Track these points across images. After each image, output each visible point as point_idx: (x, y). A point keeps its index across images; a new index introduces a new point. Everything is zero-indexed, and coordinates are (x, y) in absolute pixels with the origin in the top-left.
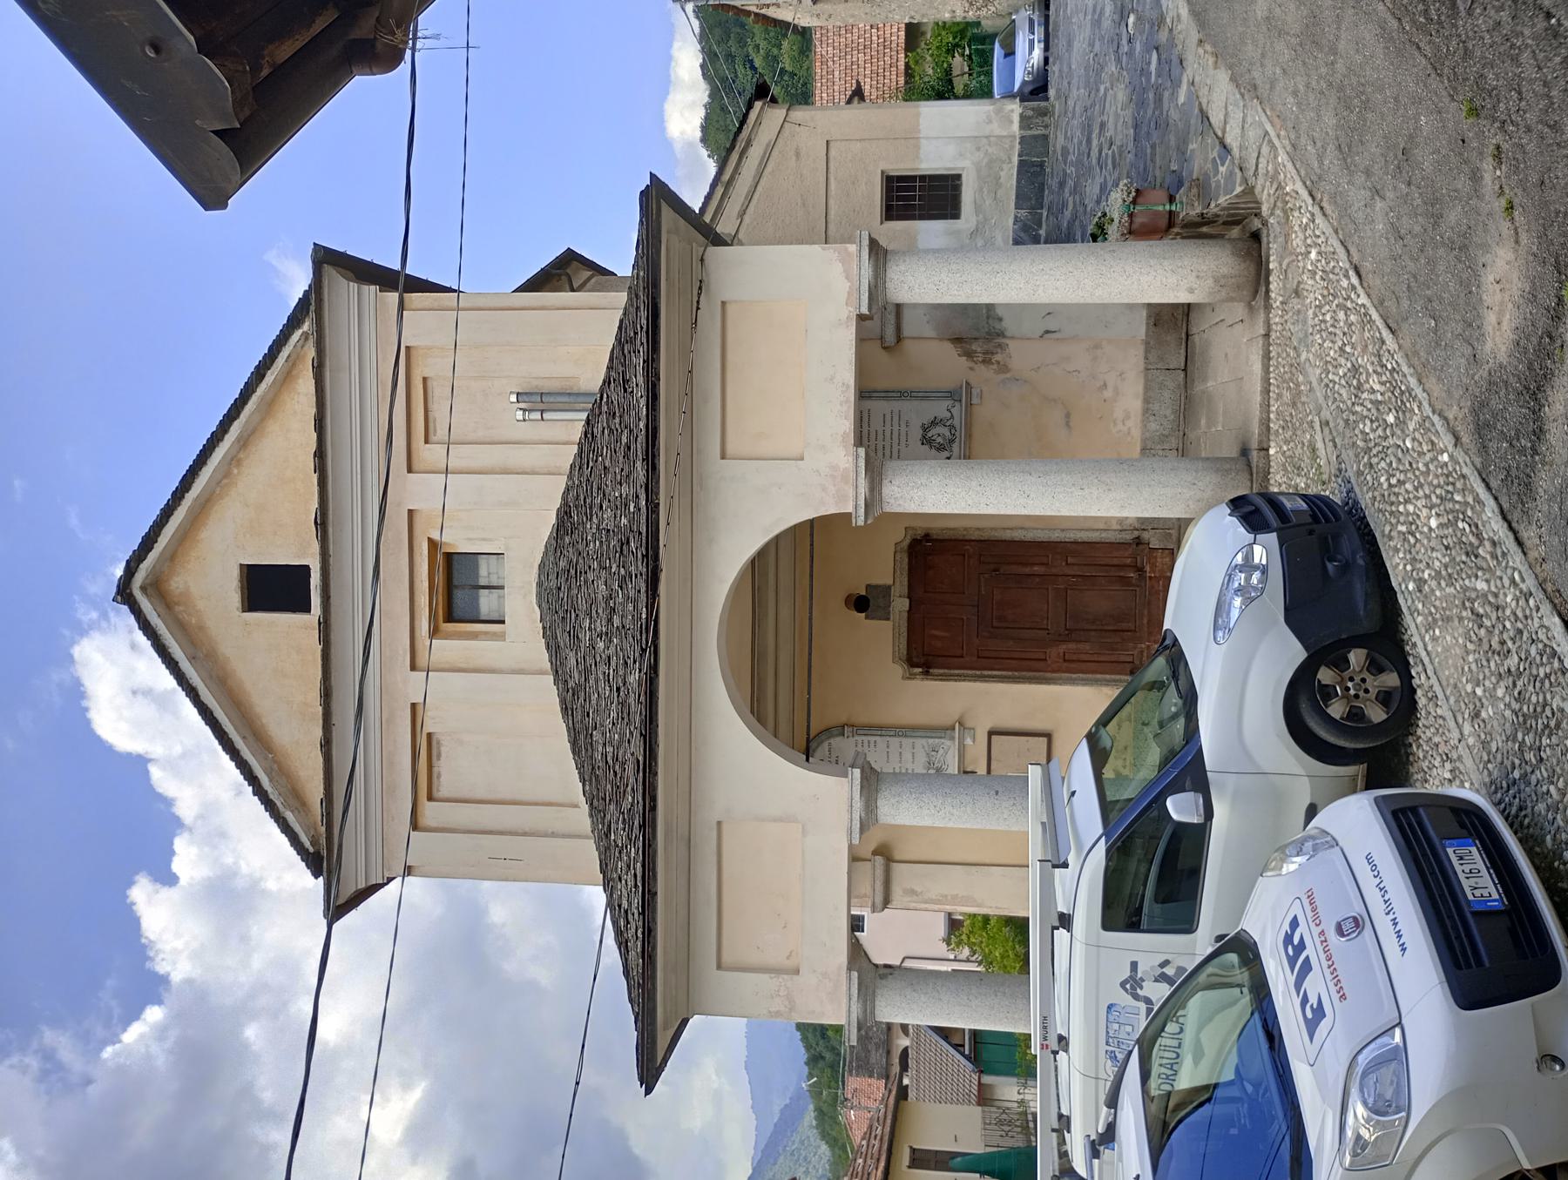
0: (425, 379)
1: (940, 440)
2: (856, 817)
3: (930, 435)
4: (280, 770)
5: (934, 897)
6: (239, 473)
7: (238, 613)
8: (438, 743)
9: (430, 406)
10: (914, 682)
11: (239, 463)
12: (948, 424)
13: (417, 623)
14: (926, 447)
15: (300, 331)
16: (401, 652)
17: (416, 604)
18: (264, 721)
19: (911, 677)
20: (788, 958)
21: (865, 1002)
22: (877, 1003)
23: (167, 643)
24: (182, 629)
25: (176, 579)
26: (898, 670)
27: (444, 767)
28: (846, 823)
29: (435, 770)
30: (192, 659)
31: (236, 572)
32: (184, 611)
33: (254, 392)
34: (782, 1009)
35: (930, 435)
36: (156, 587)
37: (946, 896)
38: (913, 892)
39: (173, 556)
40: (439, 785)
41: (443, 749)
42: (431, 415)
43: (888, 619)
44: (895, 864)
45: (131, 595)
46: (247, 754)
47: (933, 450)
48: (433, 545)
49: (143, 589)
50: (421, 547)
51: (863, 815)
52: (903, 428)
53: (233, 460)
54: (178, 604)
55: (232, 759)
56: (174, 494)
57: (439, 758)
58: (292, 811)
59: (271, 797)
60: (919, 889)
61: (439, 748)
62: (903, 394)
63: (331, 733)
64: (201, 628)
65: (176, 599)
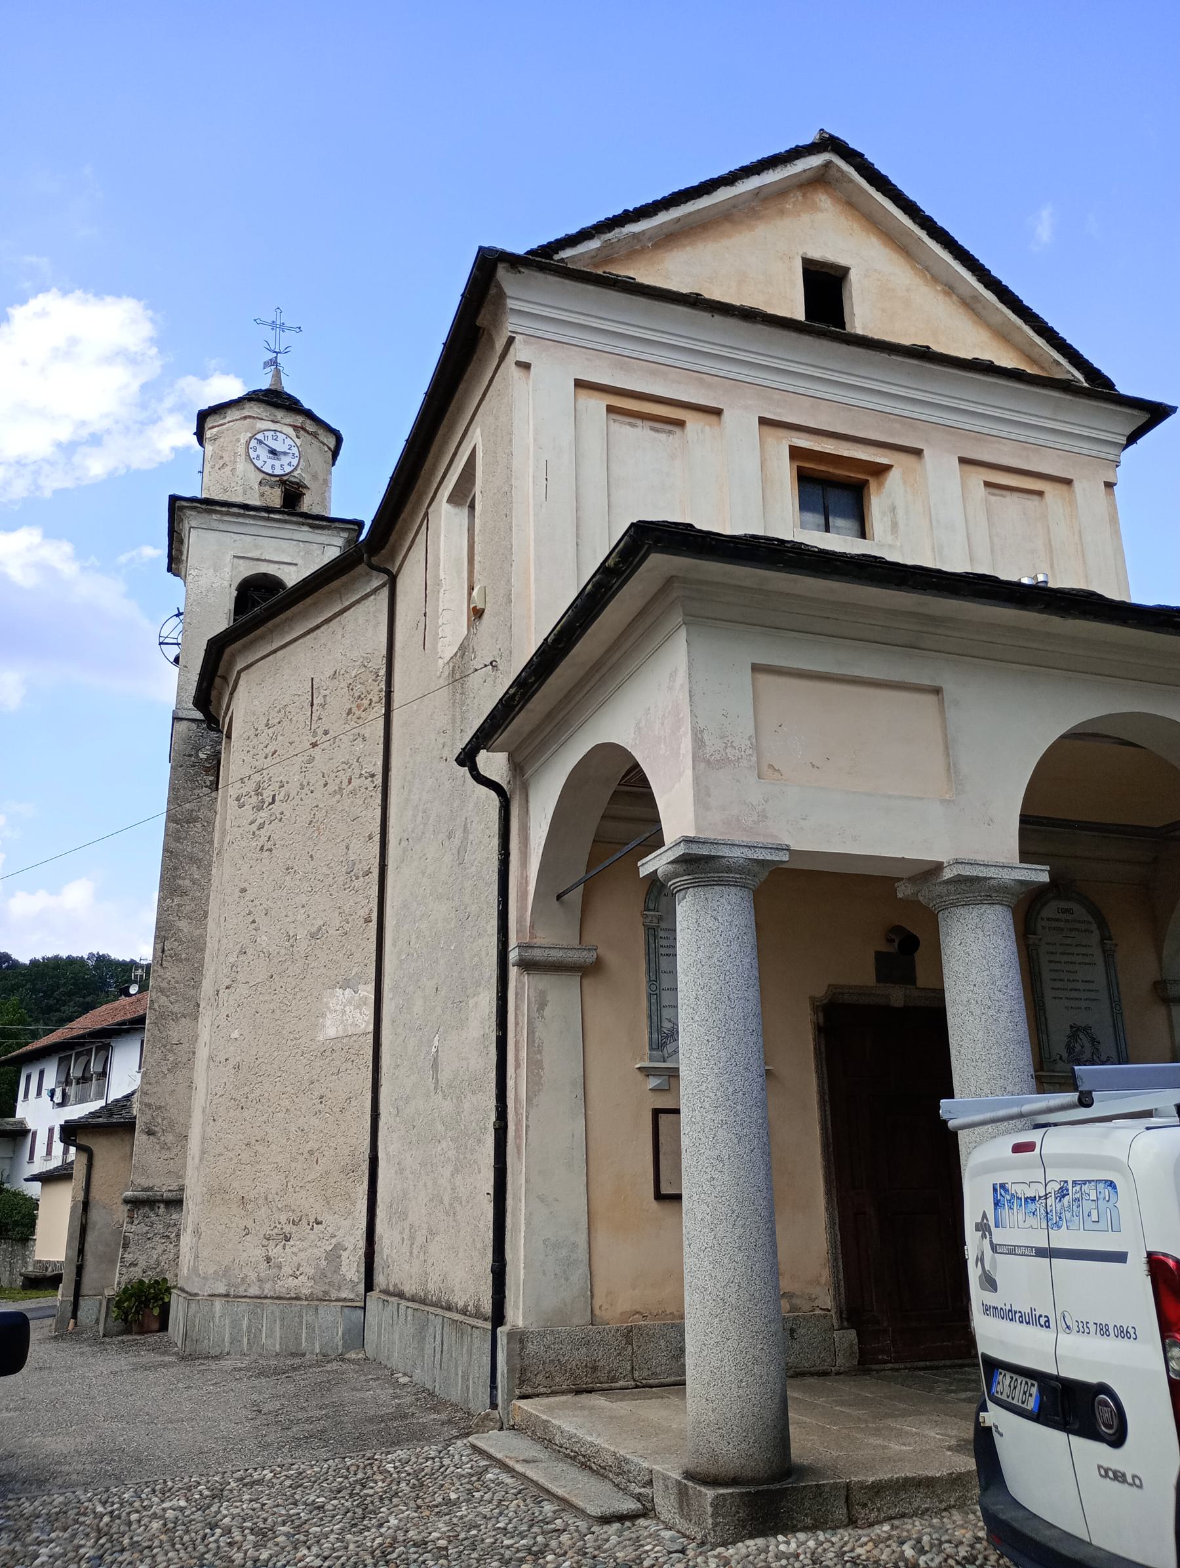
0: (1040, 494)
1: (1078, 1048)
2: (991, 873)
3: (1081, 1036)
4: (670, 238)
5: (537, 1034)
6: (937, 290)
7: (801, 253)
8: (670, 432)
9: (1016, 495)
10: (809, 1011)
11: (947, 294)
12: (1095, 1058)
13: (806, 436)
14: (1068, 1032)
15: (1083, 380)
16: (778, 410)
17: (825, 439)
18: (688, 248)
19: (815, 1009)
20: (771, 766)
21: (740, 870)
22: (733, 890)
23: (779, 169)
24: (781, 192)
25: (829, 201)
26: (820, 992)
27: (641, 433)
28: (980, 858)
29: (639, 422)
30: (757, 192)
31: (842, 261)
32: (797, 200)
33: (1026, 322)
34: (709, 750)
35: (1081, 1036)
36: (821, 180)
37: (540, 1052)
38: (542, 1006)
39: (853, 205)
40: (621, 423)
41: (663, 436)
42: (1007, 493)
43: (878, 980)
44: (579, 979)
45: (825, 150)
46: (663, 217)
47: (1067, 1040)
48: (880, 470)
49: (828, 165)
50: (882, 456)
51: (992, 882)
52: (1083, 1004)
53: (950, 288)
54: (804, 195)
55: (664, 198)
56: (930, 219)
57: (652, 429)
58: (598, 249)
59: (617, 230)
60: (547, 1011)
61: (664, 431)
62: (1115, 1003)
63: (704, 309)
64: (782, 212)
65: (809, 195)
